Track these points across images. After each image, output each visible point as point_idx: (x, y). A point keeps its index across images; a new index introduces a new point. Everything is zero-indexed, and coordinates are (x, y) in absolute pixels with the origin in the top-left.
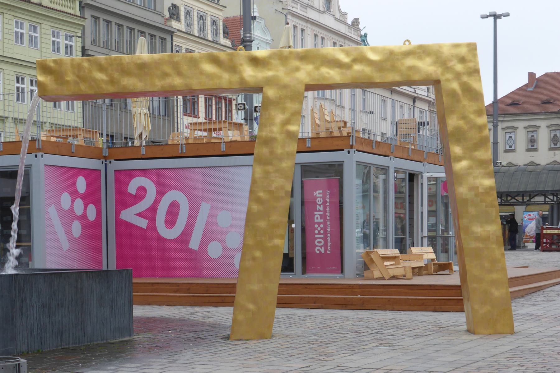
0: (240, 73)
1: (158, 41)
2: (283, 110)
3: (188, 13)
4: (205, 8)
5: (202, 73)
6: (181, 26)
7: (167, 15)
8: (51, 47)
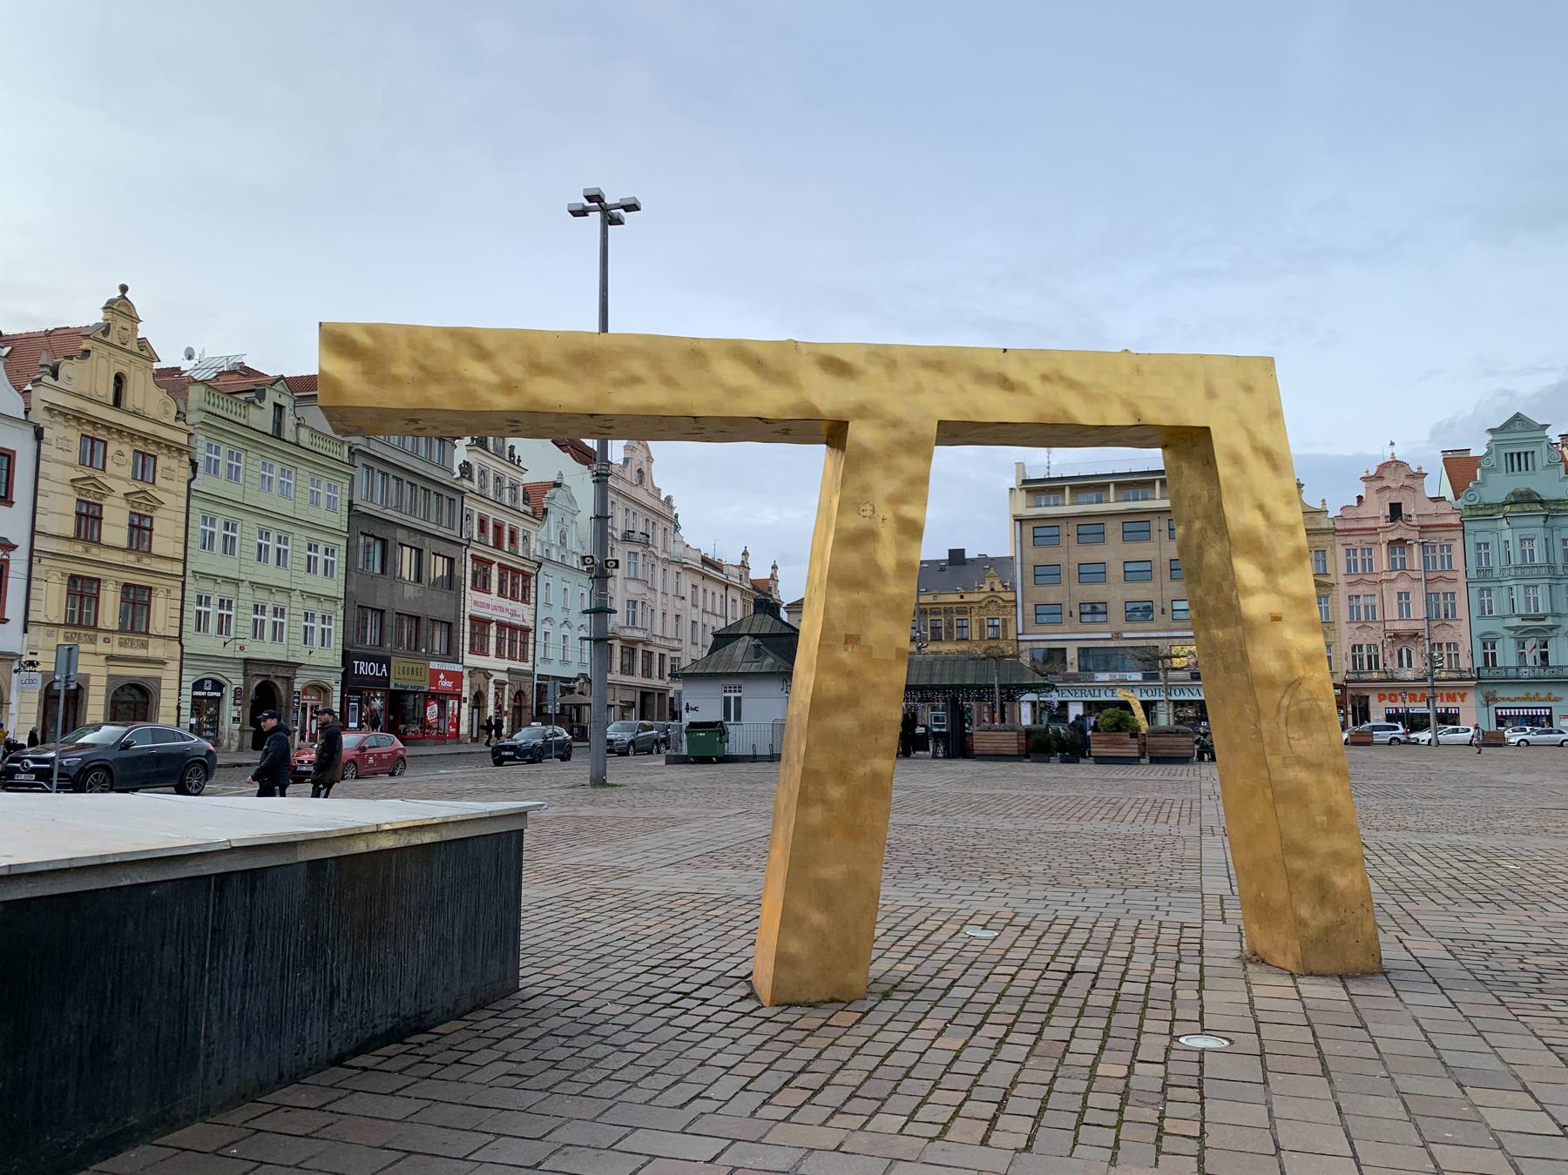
0: (798, 387)
1: (446, 502)
2: (889, 470)
3: (482, 473)
4: (504, 469)
5: (719, 383)
6: (475, 486)
7: (458, 475)
8: (308, 497)
